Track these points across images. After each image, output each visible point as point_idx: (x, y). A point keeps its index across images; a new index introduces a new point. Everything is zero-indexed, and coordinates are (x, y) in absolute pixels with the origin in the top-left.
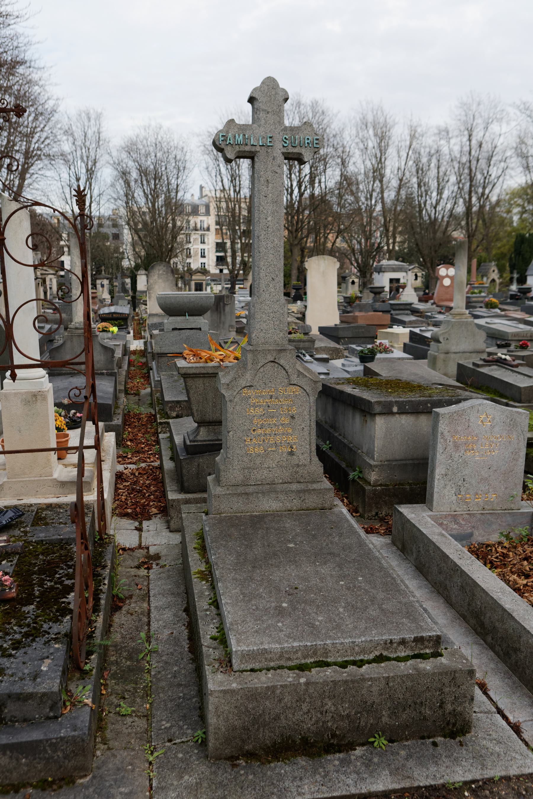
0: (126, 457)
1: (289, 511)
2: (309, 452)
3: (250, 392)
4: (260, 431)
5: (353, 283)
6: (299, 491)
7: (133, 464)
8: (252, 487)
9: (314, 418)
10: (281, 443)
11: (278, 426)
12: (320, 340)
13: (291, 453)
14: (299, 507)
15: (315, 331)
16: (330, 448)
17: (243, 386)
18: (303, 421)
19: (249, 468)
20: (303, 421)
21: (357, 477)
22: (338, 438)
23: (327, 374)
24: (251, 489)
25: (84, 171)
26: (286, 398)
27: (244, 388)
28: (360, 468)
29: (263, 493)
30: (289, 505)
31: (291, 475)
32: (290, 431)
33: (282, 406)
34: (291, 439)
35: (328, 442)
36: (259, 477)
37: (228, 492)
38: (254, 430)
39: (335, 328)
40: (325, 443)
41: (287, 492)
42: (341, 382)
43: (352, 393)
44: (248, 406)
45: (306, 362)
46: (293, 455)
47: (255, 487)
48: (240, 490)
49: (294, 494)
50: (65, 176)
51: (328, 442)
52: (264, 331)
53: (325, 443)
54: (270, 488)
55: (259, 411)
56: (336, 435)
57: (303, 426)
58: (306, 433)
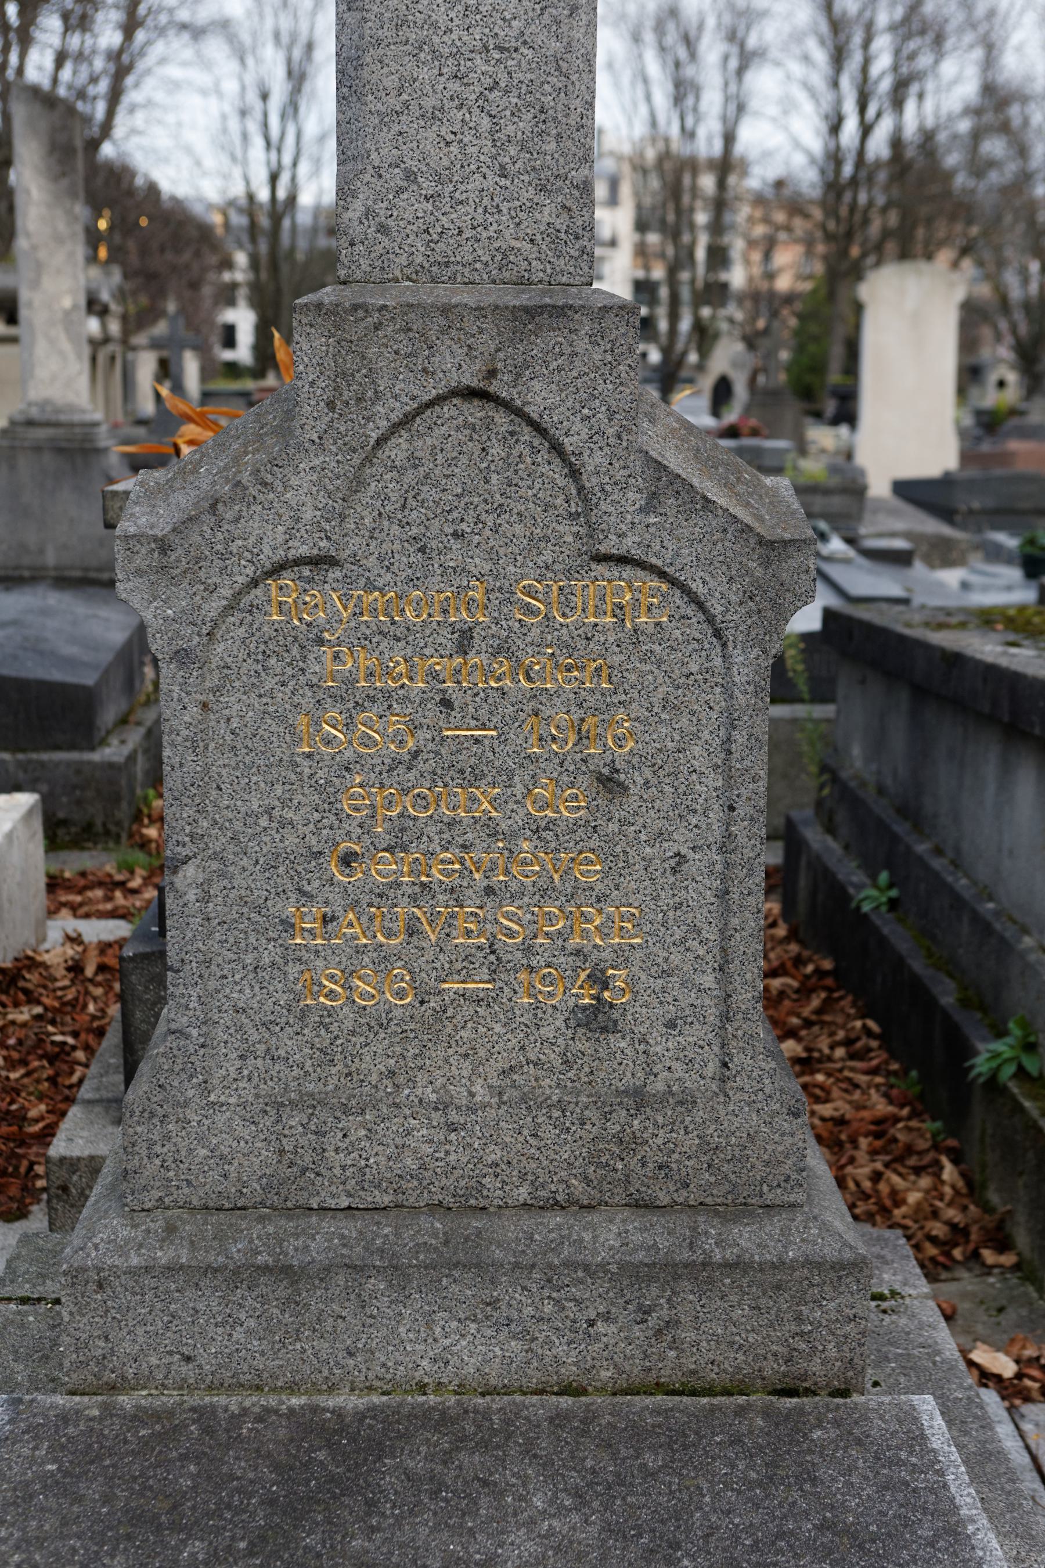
0: (122, 884)
1: (567, 1390)
2: (712, 1015)
3: (326, 603)
4: (385, 868)
5: (1001, 384)
6: (635, 1274)
7: (123, 917)
8: (329, 1226)
9: (753, 792)
10: (528, 950)
11: (511, 836)
12: (892, 512)
13: (597, 1019)
14: (635, 1369)
15: (879, 487)
16: (893, 904)
17: (268, 556)
18: (684, 810)
19: (311, 1103)
20: (684, 810)
21: (1009, 1070)
22: (927, 867)
23: (905, 601)
24: (319, 1242)
25: (279, 72)
26: (569, 648)
27: (277, 570)
28: (1024, 1025)
29: (397, 1272)
30: (566, 1357)
31: (593, 1158)
32: (590, 873)
33: (535, 704)
34: (596, 931)
35: (884, 877)
36: (378, 1160)
37: (163, 1257)
38: (347, 860)
39: (946, 481)
40: (874, 877)
41: (558, 1273)
42: (954, 620)
43: (1004, 662)
44: (307, 700)
45: (829, 559)
46: (610, 1028)
47: (350, 1228)
48: (250, 1241)
49: (603, 1286)
50: (231, 86)
51: (884, 877)
52: (428, 186)
53: (874, 877)
54: (444, 1235)
55: (382, 734)
56: (922, 848)
57: (681, 841)
58: (700, 892)
